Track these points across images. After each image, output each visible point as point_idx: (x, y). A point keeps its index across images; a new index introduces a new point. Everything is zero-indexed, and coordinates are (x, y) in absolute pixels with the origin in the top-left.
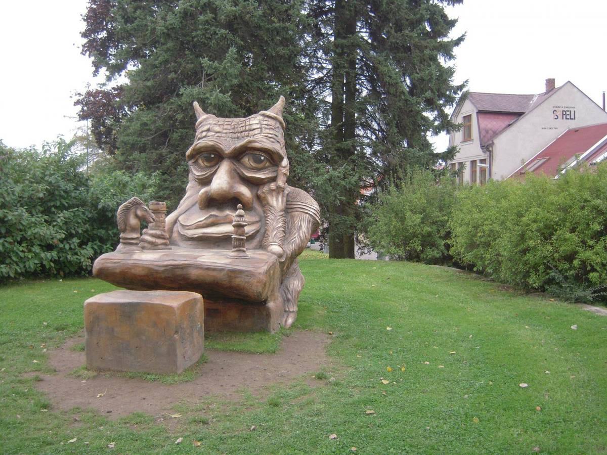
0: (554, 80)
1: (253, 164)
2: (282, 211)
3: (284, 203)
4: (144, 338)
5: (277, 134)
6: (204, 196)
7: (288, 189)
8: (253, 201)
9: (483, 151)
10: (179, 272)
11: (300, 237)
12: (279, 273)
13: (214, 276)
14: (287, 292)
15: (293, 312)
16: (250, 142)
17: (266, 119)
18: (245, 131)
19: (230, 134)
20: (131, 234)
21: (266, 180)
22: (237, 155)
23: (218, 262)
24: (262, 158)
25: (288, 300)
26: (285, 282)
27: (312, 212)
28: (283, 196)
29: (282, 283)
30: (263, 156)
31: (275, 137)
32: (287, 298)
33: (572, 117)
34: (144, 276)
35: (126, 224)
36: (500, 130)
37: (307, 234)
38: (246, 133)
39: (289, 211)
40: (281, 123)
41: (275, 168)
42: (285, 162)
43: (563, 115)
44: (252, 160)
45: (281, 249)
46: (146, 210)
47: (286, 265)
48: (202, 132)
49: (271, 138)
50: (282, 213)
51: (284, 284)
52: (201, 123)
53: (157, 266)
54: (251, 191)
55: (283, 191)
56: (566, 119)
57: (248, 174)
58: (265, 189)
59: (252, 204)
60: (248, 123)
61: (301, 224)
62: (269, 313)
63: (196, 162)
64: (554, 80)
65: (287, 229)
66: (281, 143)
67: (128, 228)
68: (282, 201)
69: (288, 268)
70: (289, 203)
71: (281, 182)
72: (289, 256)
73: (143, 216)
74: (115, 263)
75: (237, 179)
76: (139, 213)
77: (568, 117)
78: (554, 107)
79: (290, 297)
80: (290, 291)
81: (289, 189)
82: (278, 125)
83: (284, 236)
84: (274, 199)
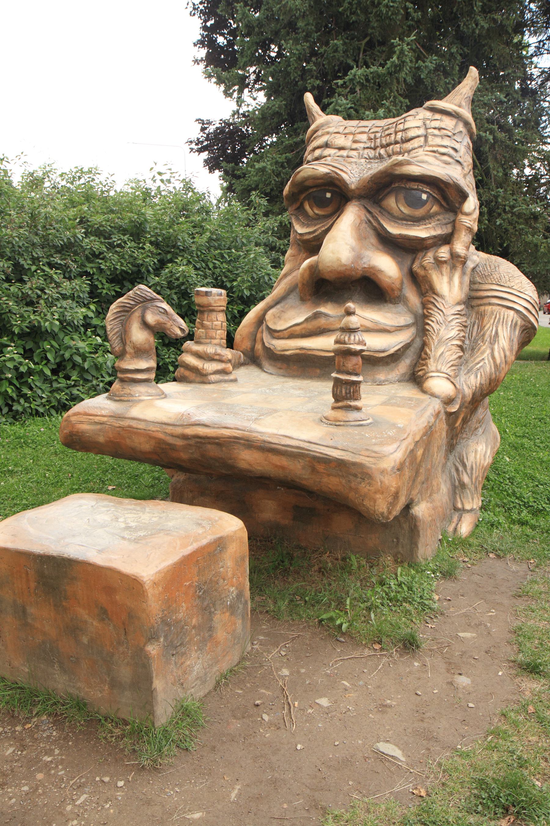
1: (406, 210)
2: (459, 304)
3: (466, 288)
4: (85, 640)
5: (457, 146)
6: (306, 275)
7: (475, 258)
8: (402, 283)
10: (213, 451)
11: (495, 362)
12: (444, 434)
13: (283, 468)
14: (461, 468)
15: (472, 510)
16: (400, 164)
17: (438, 116)
18: (396, 143)
19: (366, 151)
21: (430, 242)
23: (295, 435)
24: (424, 197)
25: (463, 486)
26: (458, 448)
27: (521, 305)
28: (463, 273)
29: (451, 447)
30: (425, 192)
31: (452, 152)
32: (460, 481)
34: (149, 452)
35: (123, 342)
37: (508, 353)
39: (475, 302)
40: (466, 124)
41: (450, 216)
42: (472, 204)
44: (403, 201)
45: (451, 386)
46: (166, 312)
47: (462, 416)
49: (443, 154)
50: (459, 308)
51: (456, 453)
52: (315, 131)
53: (172, 436)
54: (400, 264)
55: (464, 263)
57: (394, 230)
58: (429, 258)
59: (401, 290)
60: (401, 127)
61: (497, 333)
62: (416, 526)
63: (300, 209)
65: (467, 342)
66: (465, 164)
67: (128, 349)
68: (461, 283)
69: (465, 421)
70: (476, 286)
71: (462, 244)
72: (469, 398)
73: (159, 323)
74: (96, 423)
75: (373, 240)
76: (151, 318)
79: (466, 479)
80: (469, 467)
81: (477, 257)
82: (461, 127)
83: (460, 357)
84: (445, 279)
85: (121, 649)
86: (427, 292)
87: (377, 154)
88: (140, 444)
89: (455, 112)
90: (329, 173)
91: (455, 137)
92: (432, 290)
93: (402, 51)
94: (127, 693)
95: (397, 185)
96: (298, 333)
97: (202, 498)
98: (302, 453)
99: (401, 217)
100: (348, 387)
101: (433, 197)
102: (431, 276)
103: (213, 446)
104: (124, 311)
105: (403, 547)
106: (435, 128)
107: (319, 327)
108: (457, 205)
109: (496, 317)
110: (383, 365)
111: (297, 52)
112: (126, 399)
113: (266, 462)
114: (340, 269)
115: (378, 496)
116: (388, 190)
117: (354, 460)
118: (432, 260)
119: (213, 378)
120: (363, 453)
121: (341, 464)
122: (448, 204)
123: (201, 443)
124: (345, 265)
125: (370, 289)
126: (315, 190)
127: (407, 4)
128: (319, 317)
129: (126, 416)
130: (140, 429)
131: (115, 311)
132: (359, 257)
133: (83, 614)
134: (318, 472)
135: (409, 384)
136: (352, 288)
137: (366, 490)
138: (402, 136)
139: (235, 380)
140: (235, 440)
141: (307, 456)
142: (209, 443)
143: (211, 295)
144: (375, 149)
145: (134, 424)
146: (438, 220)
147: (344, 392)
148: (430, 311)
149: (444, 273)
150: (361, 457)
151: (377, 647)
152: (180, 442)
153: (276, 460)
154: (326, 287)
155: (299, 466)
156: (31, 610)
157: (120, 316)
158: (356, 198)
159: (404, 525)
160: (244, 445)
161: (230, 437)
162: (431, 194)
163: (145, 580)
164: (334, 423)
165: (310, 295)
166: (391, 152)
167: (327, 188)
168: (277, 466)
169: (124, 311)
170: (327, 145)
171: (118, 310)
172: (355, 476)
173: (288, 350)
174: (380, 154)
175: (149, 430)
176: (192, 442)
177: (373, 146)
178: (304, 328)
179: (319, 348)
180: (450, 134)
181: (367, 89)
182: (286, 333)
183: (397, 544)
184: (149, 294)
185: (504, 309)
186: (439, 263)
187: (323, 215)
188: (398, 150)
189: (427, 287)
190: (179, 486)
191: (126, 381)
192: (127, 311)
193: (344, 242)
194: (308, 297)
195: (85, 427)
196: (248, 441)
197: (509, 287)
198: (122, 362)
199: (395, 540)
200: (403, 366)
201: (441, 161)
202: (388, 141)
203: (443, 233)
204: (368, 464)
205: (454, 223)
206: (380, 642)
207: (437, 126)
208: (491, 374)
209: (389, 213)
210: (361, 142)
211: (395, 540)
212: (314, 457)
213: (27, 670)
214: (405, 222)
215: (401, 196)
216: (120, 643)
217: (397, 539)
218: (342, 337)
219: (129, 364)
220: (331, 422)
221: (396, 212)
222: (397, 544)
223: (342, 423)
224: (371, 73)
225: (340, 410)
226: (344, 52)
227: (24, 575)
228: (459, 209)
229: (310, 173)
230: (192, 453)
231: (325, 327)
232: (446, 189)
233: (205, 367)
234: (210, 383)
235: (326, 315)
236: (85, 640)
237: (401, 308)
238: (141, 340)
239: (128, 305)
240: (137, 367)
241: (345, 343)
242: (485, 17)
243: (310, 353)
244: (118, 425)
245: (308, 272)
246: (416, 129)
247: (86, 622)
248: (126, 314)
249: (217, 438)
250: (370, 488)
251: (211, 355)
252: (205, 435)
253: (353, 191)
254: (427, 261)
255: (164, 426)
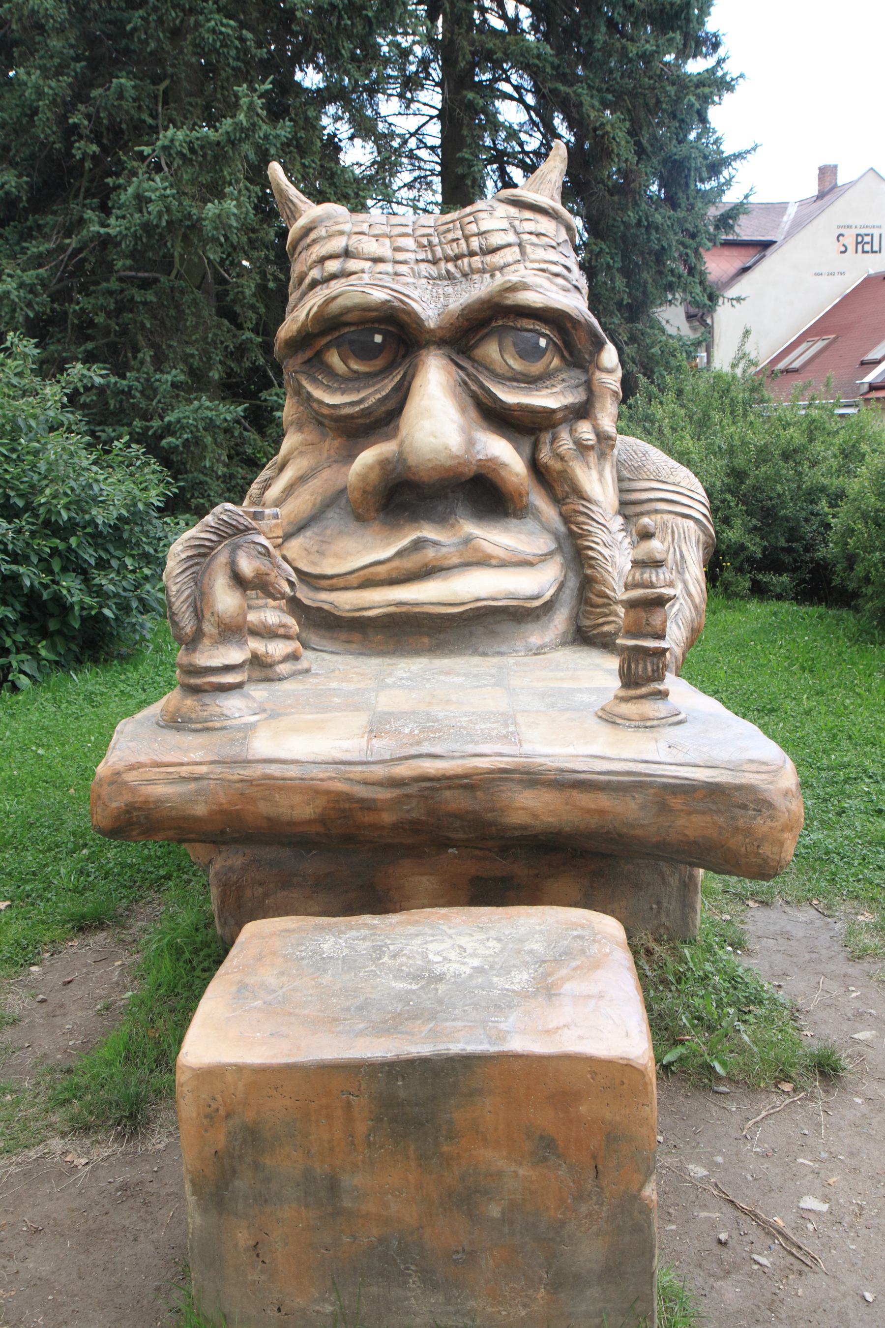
0: (836, 167)
1: (516, 364)
6: (374, 476)
9: (691, 327)
10: (455, 801)
11: (693, 601)
13: (601, 812)
16: (514, 288)
17: (528, 214)
18: (472, 254)
19: (423, 266)
20: (222, 649)
21: (560, 415)
22: (473, 331)
24: (543, 342)
33: (876, 248)
35: (198, 615)
36: (725, 279)
38: (477, 261)
43: (857, 243)
44: (511, 349)
48: (322, 260)
49: (557, 275)
53: (366, 783)
56: (864, 252)
57: (509, 396)
64: (836, 167)
67: (207, 628)
70: (626, 485)
71: (607, 416)
74: (184, 779)
77: (867, 248)
78: (839, 227)
82: (563, 235)
84: (594, 474)
85: (584, 1209)
86: (567, 497)
87: (444, 272)
88: (292, 807)
89: (553, 209)
90: (389, 301)
91: (560, 249)
92: (579, 493)
93: (251, 107)
94: (593, 1292)
95: (500, 323)
96: (382, 577)
97: (285, 893)
98: (640, 782)
99: (509, 375)
100: (655, 660)
101: (555, 344)
102: (573, 470)
103: (456, 792)
104: (200, 555)
105: (668, 915)
106: (531, 233)
107: (426, 565)
108: (587, 357)
109: (673, 532)
110: (533, 621)
111: (51, 92)
112: (218, 725)
113: (568, 807)
114: (449, 463)
115: (786, 835)
116: (486, 331)
117: (737, 782)
118: (572, 446)
119: (283, 669)
120: (746, 767)
121: (715, 792)
122: (571, 354)
123: (432, 789)
124: (457, 457)
125: (484, 494)
126: (353, 329)
127: (244, 32)
128: (424, 548)
129: (250, 757)
130: (291, 779)
131: (184, 556)
132: (471, 442)
133: (494, 1158)
134: (671, 811)
135: (575, 648)
136: (451, 495)
137: (765, 829)
138: (480, 244)
139: (308, 671)
140: (503, 776)
141: (650, 785)
142: (449, 788)
143: (263, 519)
144: (435, 262)
145: (274, 770)
146: (563, 380)
147: (649, 669)
148: (586, 527)
149: (592, 465)
150: (746, 774)
151: (787, 1087)
152: (385, 794)
153: (586, 800)
154: (405, 496)
155: (633, 805)
156: (351, 1181)
157: (192, 566)
158: (434, 343)
159: (671, 879)
160: (521, 781)
161: (491, 772)
162: (551, 339)
163: (641, 1061)
164: (641, 724)
165: (377, 510)
166: (467, 268)
167: (376, 325)
168: (589, 811)
169: (200, 555)
170: (347, 254)
171: (189, 553)
172: (744, 807)
173: (369, 608)
174: (448, 271)
175: (312, 779)
176: (412, 790)
177: (430, 257)
178: (396, 568)
179: (434, 599)
180: (554, 244)
181: (193, 166)
182: (353, 580)
183: (659, 912)
184: (241, 520)
185: (680, 519)
186: (582, 448)
187: (367, 373)
188: (480, 266)
189: (567, 489)
190: (234, 878)
191: (206, 691)
192: (204, 555)
193: (437, 420)
194: (373, 514)
195: (161, 790)
196: (528, 773)
197: (674, 484)
198: (197, 654)
199: (654, 906)
200: (560, 621)
201: (557, 285)
202: (456, 251)
203: (577, 401)
204: (764, 786)
205: (589, 386)
206: (788, 1079)
207: (533, 230)
208: (693, 620)
209: (487, 369)
210: (407, 251)
211: (654, 906)
212: (665, 786)
213: (329, 1309)
214: (515, 384)
215: (509, 341)
216: (580, 1197)
217: (659, 903)
218: (646, 576)
219: (211, 657)
220: (637, 723)
221: (501, 369)
222: (659, 912)
223: (655, 723)
224: (198, 139)
225: (643, 701)
226: (134, 101)
227: (339, 1113)
228: (590, 362)
229: (357, 301)
230: (408, 811)
231: (435, 563)
232: (574, 332)
233: (270, 652)
234: (280, 680)
235: (436, 543)
236: (495, 1210)
237: (530, 524)
238: (232, 610)
239: (208, 544)
240: (227, 662)
241: (652, 586)
242: (359, 67)
243: (417, 610)
244: (236, 777)
245: (377, 471)
246: (502, 233)
247: (500, 1174)
248: (202, 560)
249: (466, 776)
250: (774, 824)
251: (274, 628)
252: (441, 773)
253: (431, 331)
254: (566, 447)
255: (342, 767)
